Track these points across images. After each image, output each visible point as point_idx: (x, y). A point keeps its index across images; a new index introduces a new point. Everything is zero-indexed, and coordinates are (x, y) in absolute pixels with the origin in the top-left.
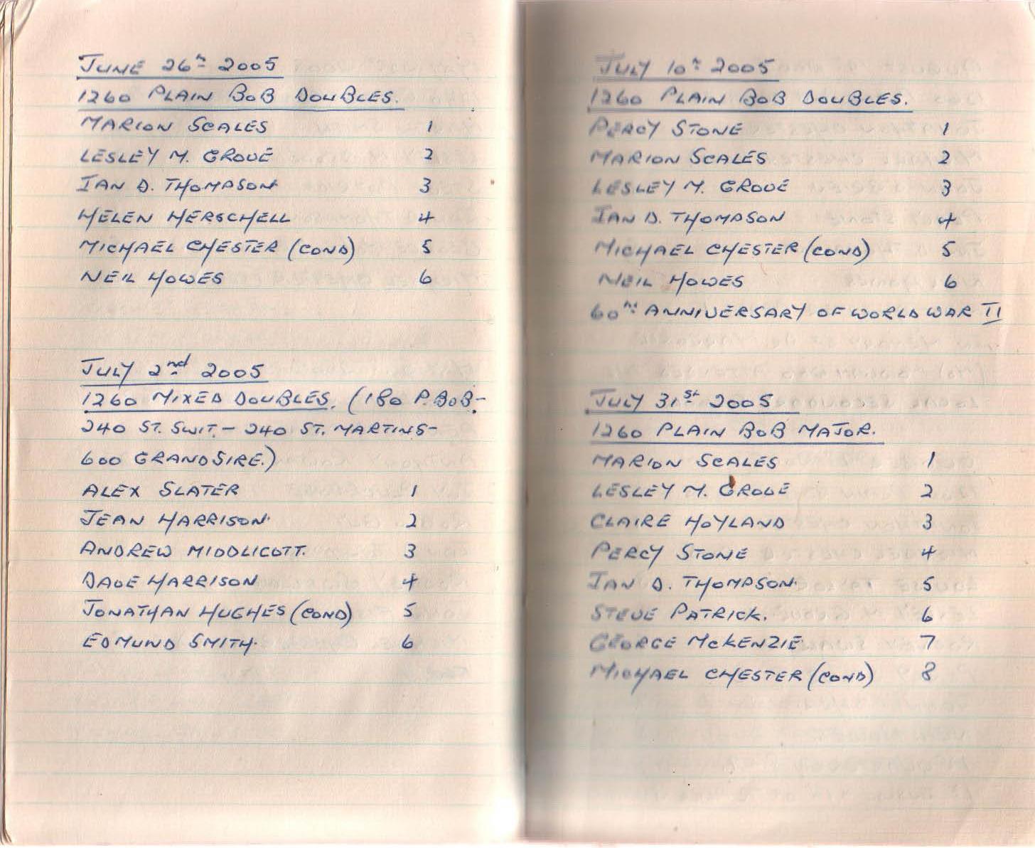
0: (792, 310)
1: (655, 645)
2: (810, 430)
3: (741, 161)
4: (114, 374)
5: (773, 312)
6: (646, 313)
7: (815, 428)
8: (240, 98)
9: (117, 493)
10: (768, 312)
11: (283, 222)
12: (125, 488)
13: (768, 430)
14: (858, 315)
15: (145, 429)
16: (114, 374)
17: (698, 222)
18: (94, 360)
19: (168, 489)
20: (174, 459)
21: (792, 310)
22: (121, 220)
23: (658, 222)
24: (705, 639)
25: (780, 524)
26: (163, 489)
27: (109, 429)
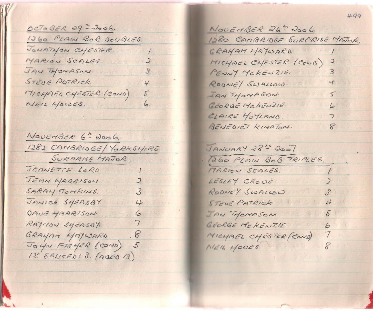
0: (244, 126)
1: (211, 52)
2: (46, 224)
5: (234, 149)
6: (39, 181)
7: (339, 38)
10: (224, 51)
13: (94, 39)
14: (256, 85)
15: (249, 171)
17: (59, 51)
18: (240, 33)
19: (264, 94)
20: (267, 117)
21: (242, 147)
23: (291, 53)
24: (67, 71)
25: (315, 64)
26: (262, 94)
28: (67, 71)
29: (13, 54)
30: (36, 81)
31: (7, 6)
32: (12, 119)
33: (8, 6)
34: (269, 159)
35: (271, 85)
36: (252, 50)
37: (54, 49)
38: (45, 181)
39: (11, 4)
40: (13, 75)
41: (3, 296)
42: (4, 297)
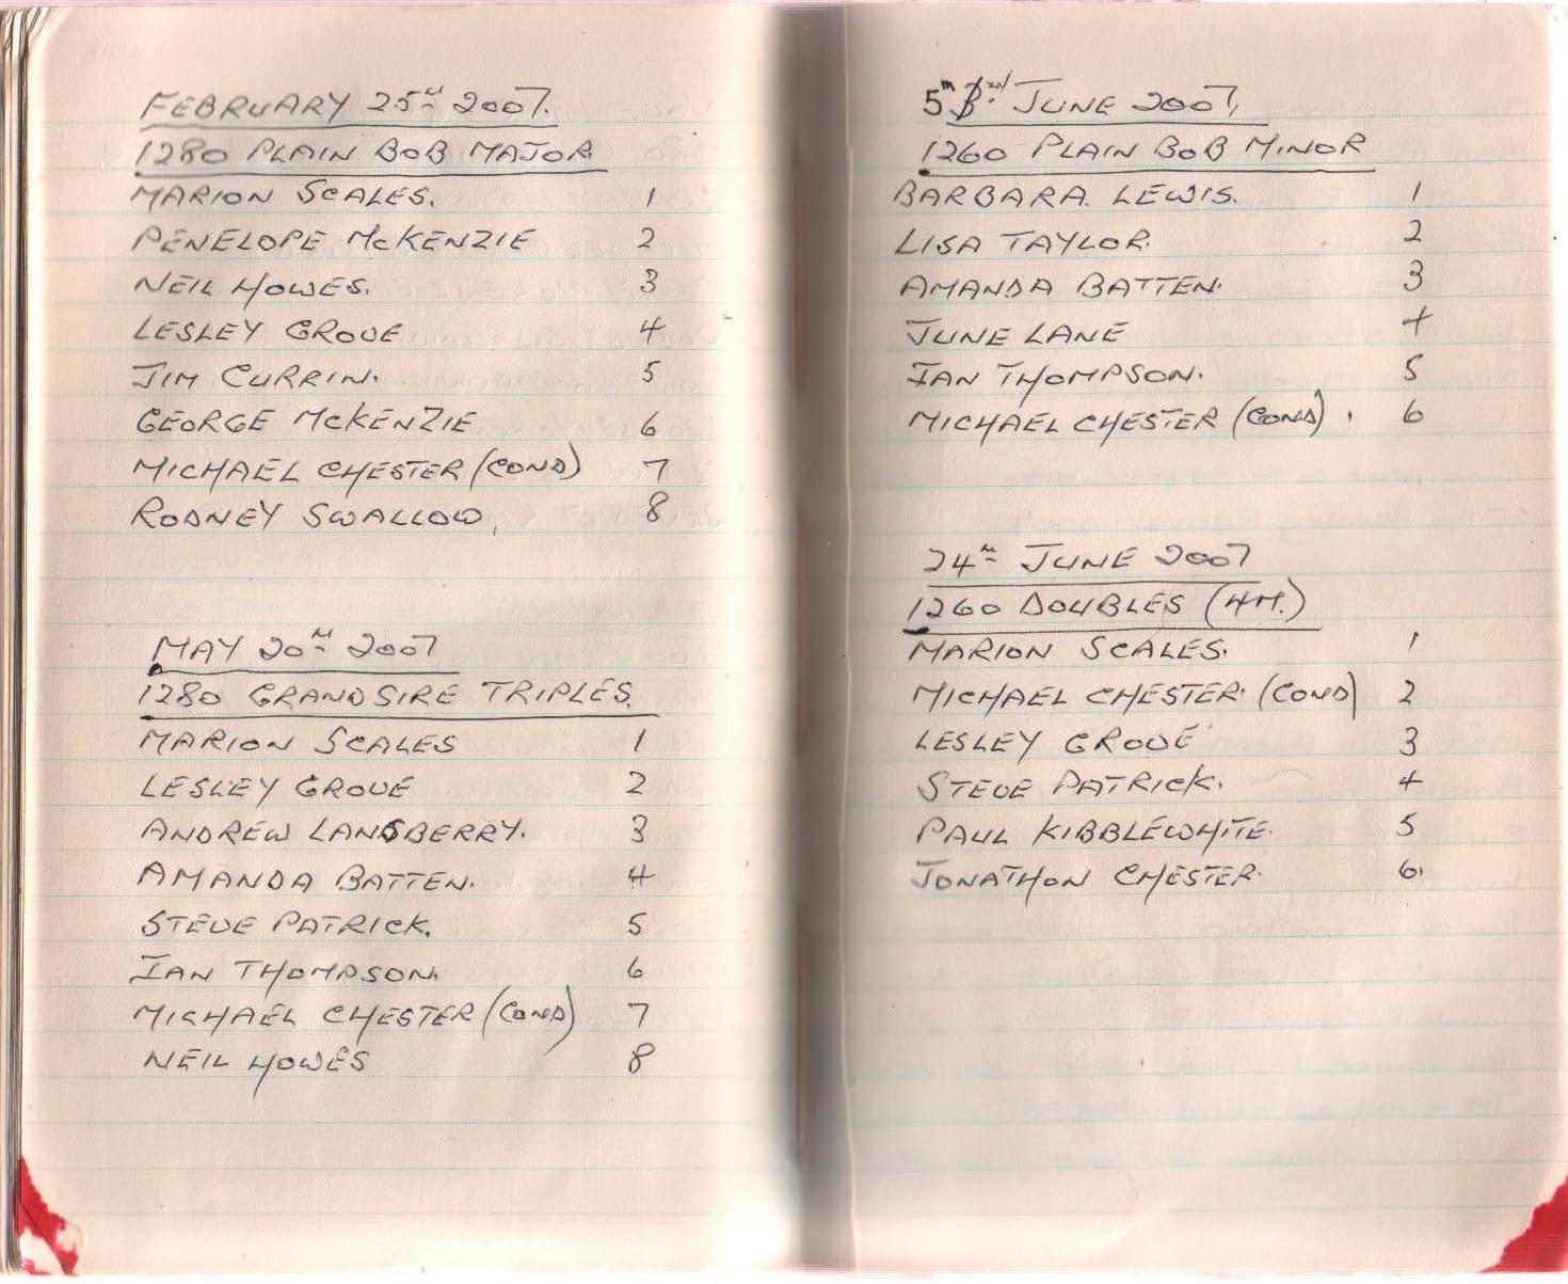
3: (1141, 835)
4: (203, 291)
8: (1416, 285)
9: (999, 746)
11: (151, 1057)
12: (235, 233)
16: (203, 291)
22: (989, 747)
24: (993, 423)
27: (924, 383)
28: (993, 423)
29: (54, 214)
30: (261, 962)
31: (26, 16)
32: (53, 534)
33: (29, 15)
34: (1114, 605)
35: (981, 744)
36: (1023, 375)
37: (265, 964)
38: (187, 246)
39: (44, 12)
40: (54, 305)
41: (19, 1231)
42: (22, 1232)
